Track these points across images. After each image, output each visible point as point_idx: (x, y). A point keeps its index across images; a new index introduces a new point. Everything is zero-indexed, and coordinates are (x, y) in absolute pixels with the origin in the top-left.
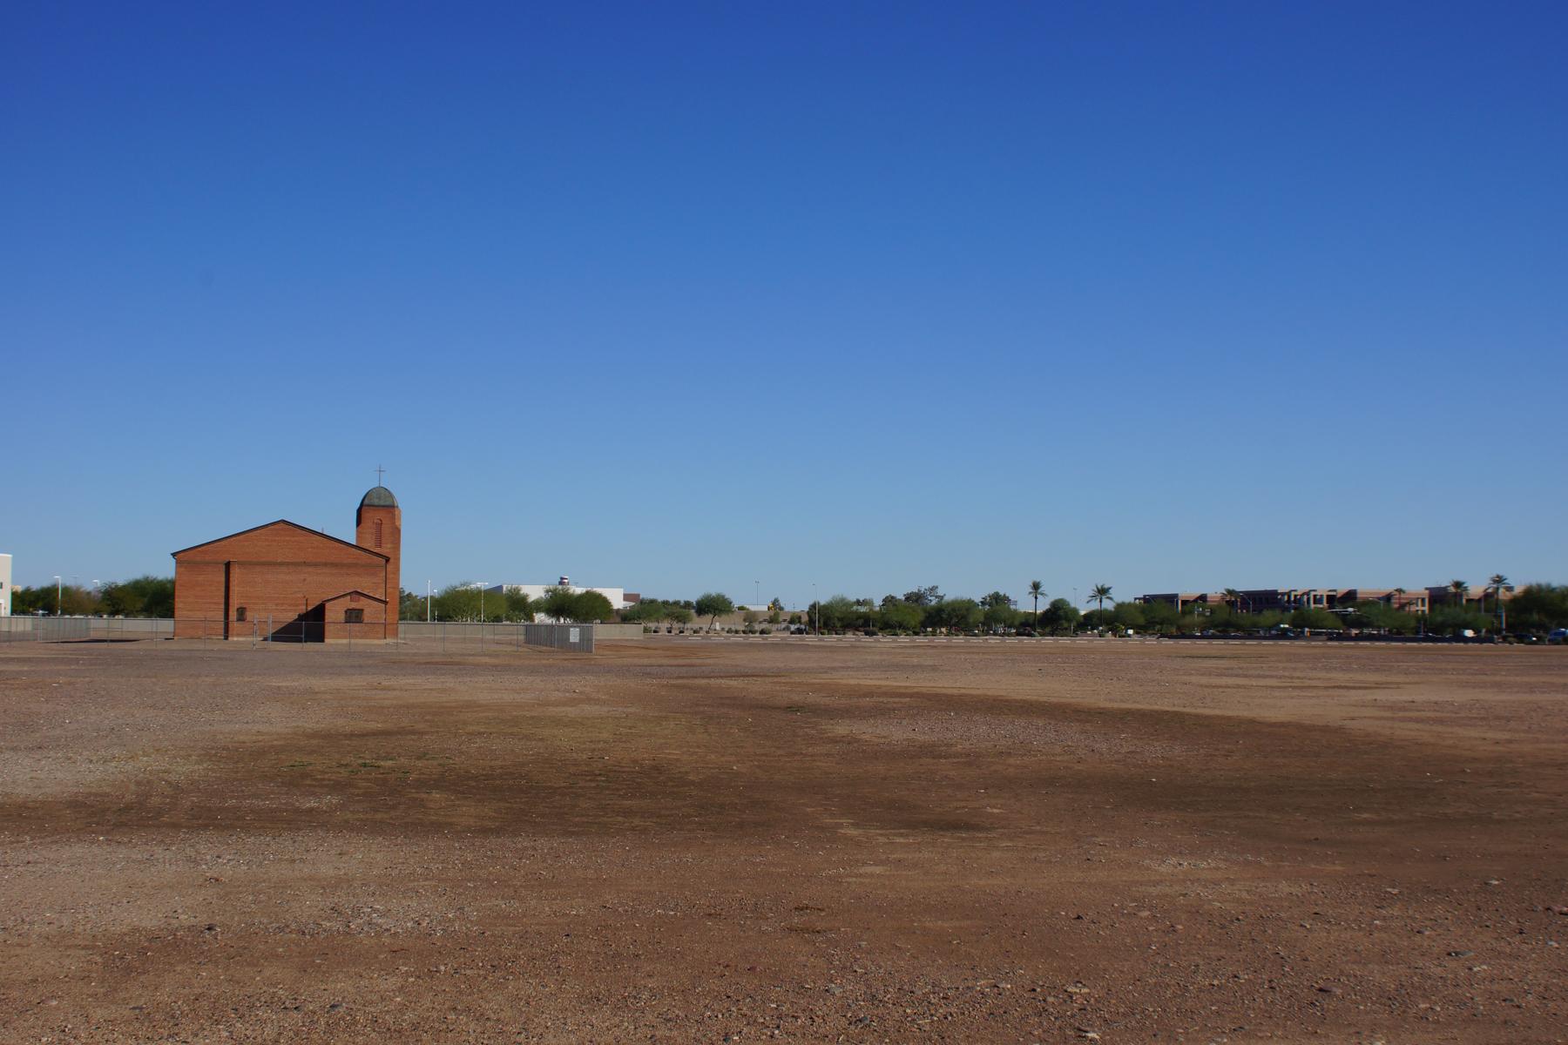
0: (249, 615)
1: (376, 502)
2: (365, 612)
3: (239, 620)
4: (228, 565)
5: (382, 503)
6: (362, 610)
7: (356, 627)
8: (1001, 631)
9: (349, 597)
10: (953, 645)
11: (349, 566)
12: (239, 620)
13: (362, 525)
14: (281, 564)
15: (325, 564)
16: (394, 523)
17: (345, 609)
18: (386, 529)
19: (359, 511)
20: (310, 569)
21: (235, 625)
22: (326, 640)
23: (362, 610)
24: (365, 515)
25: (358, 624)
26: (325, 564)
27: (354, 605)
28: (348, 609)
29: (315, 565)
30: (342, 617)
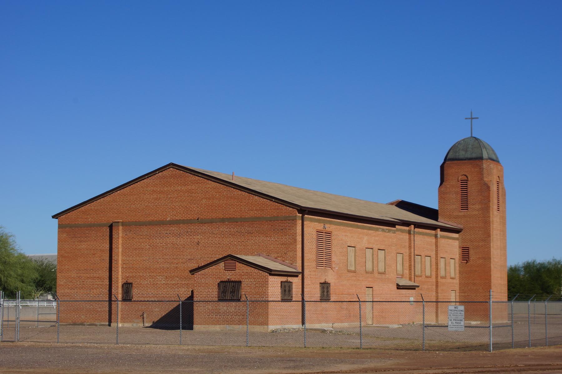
0: (136, 293)
1: (462, 154)
2: (243, 285)
3: (124, 300)
4: (111, 227)
5: (468, 155)
6: (240, 282)
7: (231, 307)
8: (168, 354)
9: (222, 265)
10: (434, 274)
11: (253, 220)
12: (124, 300)
13: (443, 185)
14: (173, 223)
15: (223, 221)
16: (482, 179)
17: (219, 281)
18: (473, 187)
19: (442, 167)
20: (205, 228)
21: (120, 306)
22: (195, 326)
23: (240, 282)
24: (450, 171)
25: (234, 303)
26: (223, 221)
27: (229, 276)
28: (221, 282)
29: (211, 222)
30: (214, 292)
